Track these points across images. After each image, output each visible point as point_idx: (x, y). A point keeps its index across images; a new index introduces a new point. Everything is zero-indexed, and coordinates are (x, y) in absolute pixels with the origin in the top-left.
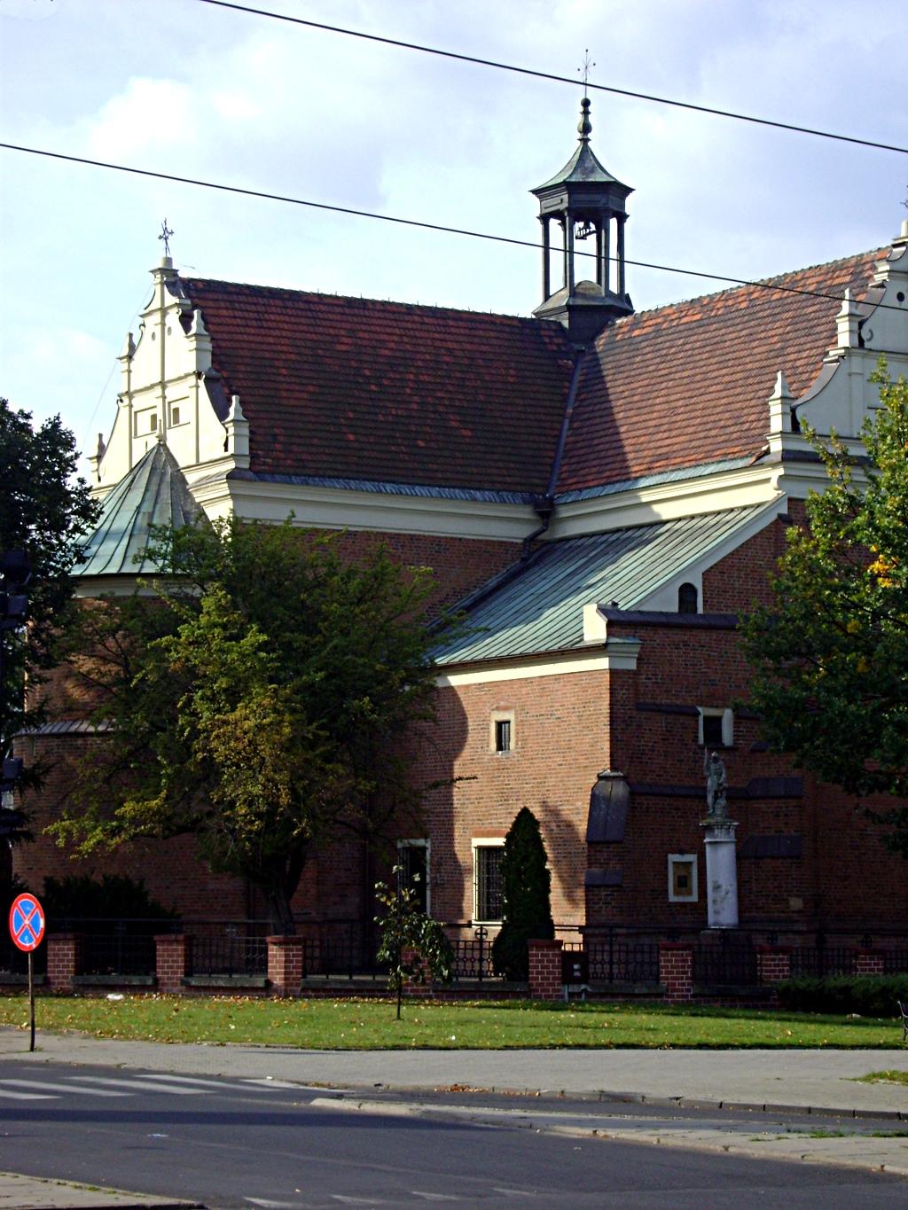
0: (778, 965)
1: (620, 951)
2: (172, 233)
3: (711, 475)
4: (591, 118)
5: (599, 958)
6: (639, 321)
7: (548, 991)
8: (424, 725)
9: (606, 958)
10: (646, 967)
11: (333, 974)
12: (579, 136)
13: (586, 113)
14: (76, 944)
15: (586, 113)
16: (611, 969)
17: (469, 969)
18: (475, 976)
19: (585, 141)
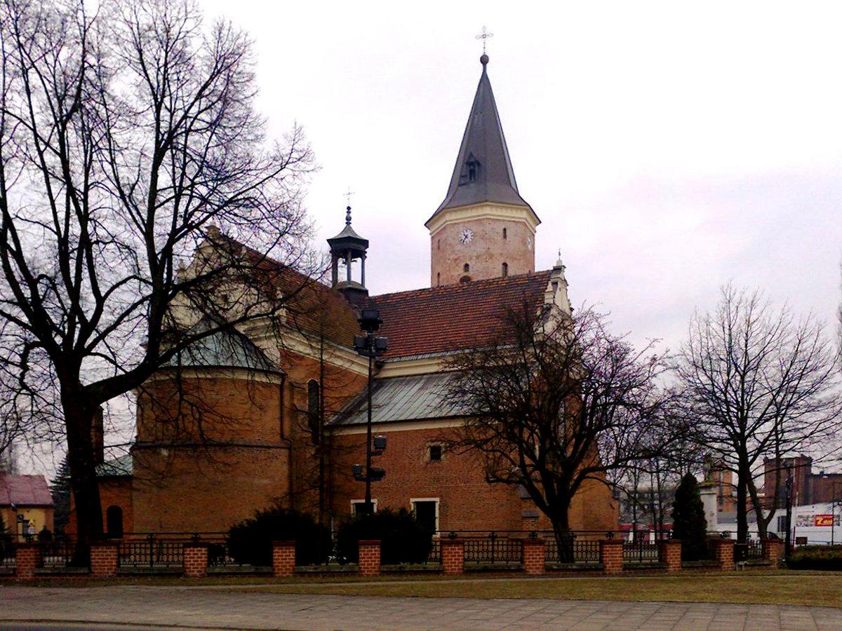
0: (100, 559)
1: (503, 545)
2: (203, 11)
3: (412, 367)
4: (351, 215)
5: (500, 548)
6: (18, 476)
7: (372, 564)
8: (695, 344)
9: (496, 548)
10: (143, 557)
11: (244, 563)
12: (346, 221)
13: (349, 212)
14: (296, 549)
15: (349, 212)
16: (151, 558)
17: (551, 556)
18: (555, 561)
19: (348, 223)
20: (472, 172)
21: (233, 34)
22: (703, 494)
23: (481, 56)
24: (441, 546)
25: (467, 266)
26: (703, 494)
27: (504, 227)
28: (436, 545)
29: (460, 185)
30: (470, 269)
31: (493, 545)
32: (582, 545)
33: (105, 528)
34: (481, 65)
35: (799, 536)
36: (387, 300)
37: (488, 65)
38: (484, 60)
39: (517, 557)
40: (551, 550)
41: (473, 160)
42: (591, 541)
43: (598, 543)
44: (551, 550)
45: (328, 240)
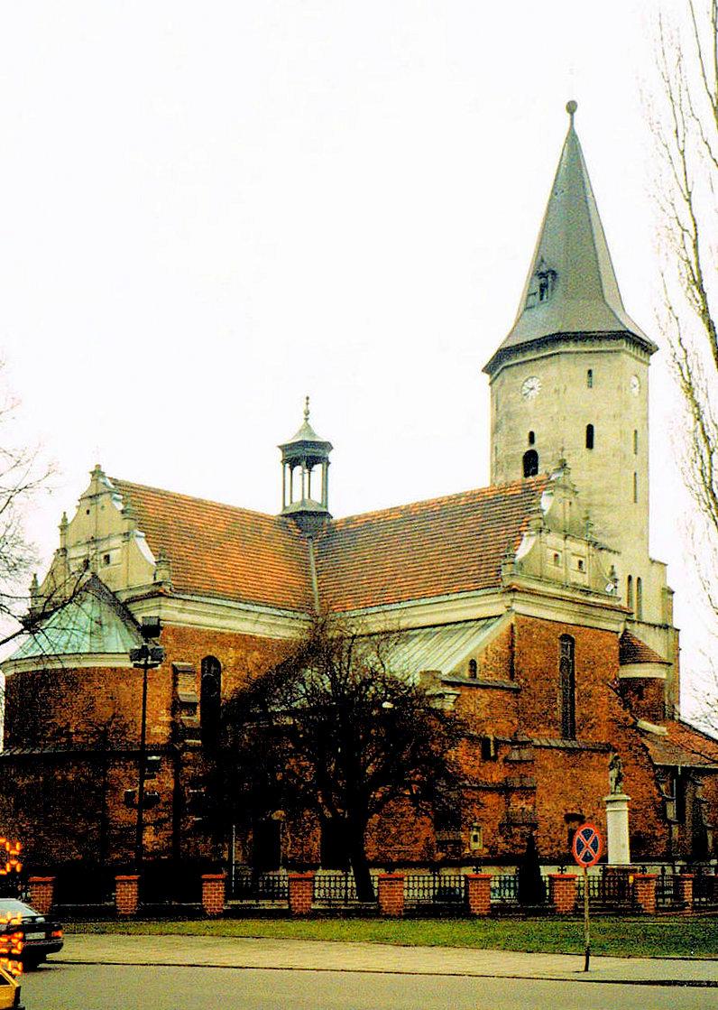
12: (304, 416)
20: (543, 287)
21: (11, 603)
22: (122, 882)
23: (567, 101)
24: (466, 882)
25: (532, 436)
26: (122, 882)
27: (589, 368)
28: (374, 881)
29: (528, 308)
30: (537, 441)
31: (440, 881)
32: (450, 881)
33: (197, 741)
34: (569, 115)
35: (629, 858)
36: (368, 525)
37: (575, 114)
38: (571, 108)
39: (341, 895)
40: (426, 886)
41: (544, 269)
42: (413, 876)
43: (463, 879)
44: (426, 886)
45: (280, 447)
